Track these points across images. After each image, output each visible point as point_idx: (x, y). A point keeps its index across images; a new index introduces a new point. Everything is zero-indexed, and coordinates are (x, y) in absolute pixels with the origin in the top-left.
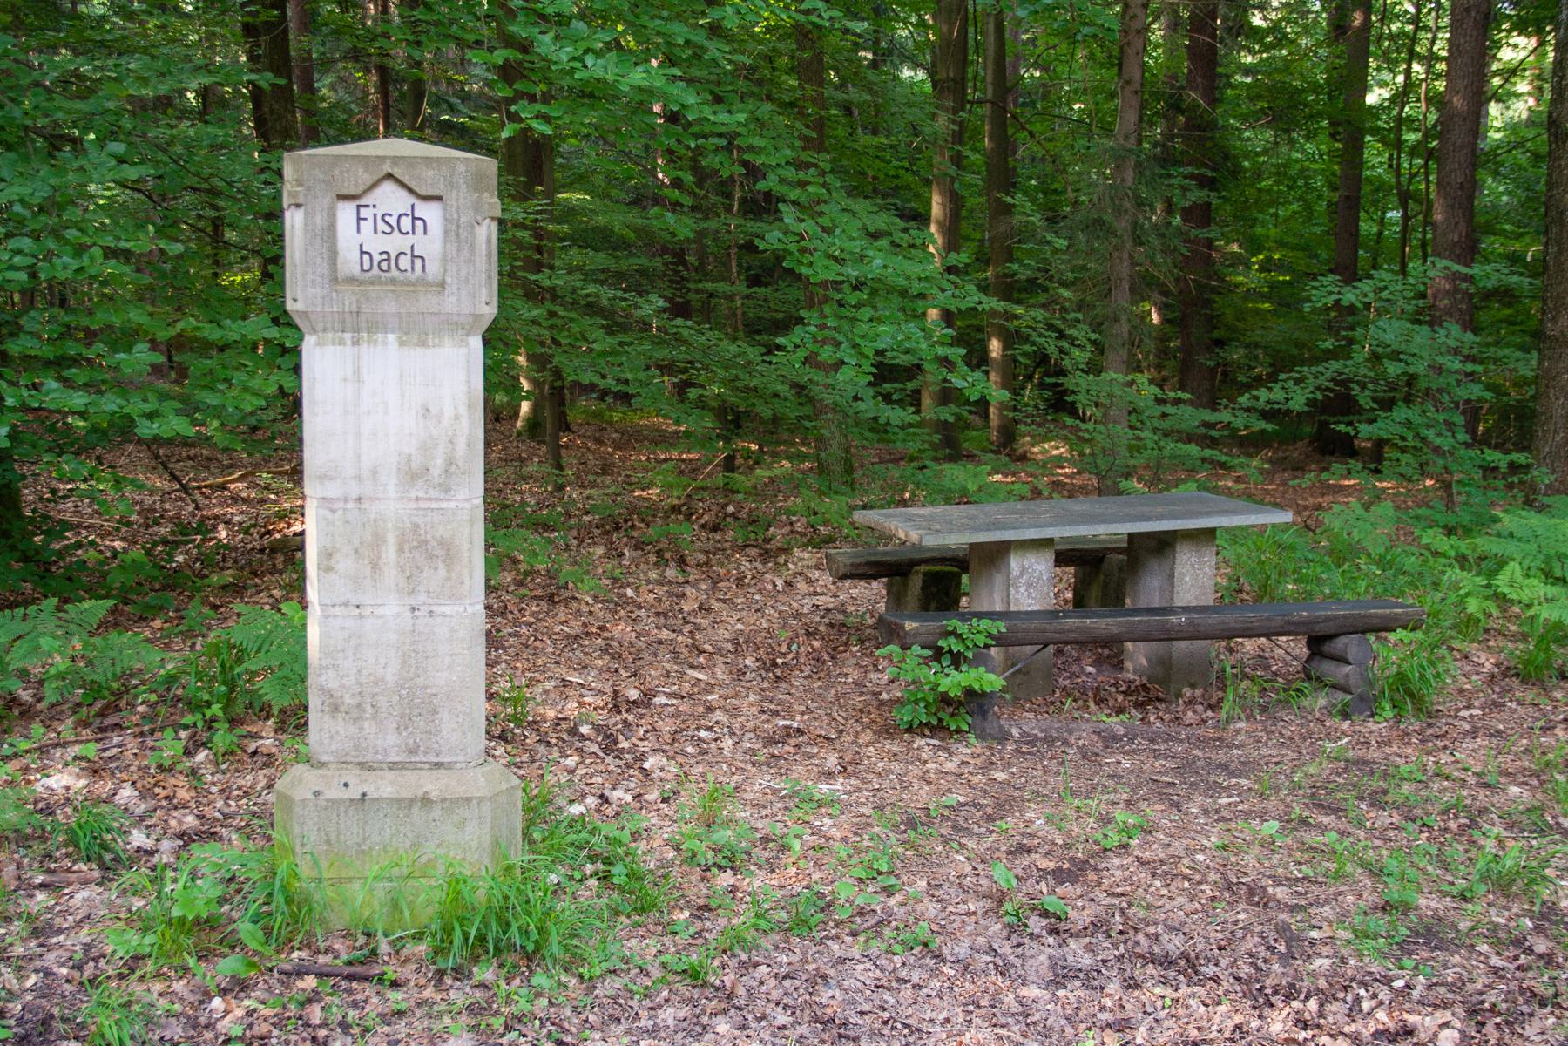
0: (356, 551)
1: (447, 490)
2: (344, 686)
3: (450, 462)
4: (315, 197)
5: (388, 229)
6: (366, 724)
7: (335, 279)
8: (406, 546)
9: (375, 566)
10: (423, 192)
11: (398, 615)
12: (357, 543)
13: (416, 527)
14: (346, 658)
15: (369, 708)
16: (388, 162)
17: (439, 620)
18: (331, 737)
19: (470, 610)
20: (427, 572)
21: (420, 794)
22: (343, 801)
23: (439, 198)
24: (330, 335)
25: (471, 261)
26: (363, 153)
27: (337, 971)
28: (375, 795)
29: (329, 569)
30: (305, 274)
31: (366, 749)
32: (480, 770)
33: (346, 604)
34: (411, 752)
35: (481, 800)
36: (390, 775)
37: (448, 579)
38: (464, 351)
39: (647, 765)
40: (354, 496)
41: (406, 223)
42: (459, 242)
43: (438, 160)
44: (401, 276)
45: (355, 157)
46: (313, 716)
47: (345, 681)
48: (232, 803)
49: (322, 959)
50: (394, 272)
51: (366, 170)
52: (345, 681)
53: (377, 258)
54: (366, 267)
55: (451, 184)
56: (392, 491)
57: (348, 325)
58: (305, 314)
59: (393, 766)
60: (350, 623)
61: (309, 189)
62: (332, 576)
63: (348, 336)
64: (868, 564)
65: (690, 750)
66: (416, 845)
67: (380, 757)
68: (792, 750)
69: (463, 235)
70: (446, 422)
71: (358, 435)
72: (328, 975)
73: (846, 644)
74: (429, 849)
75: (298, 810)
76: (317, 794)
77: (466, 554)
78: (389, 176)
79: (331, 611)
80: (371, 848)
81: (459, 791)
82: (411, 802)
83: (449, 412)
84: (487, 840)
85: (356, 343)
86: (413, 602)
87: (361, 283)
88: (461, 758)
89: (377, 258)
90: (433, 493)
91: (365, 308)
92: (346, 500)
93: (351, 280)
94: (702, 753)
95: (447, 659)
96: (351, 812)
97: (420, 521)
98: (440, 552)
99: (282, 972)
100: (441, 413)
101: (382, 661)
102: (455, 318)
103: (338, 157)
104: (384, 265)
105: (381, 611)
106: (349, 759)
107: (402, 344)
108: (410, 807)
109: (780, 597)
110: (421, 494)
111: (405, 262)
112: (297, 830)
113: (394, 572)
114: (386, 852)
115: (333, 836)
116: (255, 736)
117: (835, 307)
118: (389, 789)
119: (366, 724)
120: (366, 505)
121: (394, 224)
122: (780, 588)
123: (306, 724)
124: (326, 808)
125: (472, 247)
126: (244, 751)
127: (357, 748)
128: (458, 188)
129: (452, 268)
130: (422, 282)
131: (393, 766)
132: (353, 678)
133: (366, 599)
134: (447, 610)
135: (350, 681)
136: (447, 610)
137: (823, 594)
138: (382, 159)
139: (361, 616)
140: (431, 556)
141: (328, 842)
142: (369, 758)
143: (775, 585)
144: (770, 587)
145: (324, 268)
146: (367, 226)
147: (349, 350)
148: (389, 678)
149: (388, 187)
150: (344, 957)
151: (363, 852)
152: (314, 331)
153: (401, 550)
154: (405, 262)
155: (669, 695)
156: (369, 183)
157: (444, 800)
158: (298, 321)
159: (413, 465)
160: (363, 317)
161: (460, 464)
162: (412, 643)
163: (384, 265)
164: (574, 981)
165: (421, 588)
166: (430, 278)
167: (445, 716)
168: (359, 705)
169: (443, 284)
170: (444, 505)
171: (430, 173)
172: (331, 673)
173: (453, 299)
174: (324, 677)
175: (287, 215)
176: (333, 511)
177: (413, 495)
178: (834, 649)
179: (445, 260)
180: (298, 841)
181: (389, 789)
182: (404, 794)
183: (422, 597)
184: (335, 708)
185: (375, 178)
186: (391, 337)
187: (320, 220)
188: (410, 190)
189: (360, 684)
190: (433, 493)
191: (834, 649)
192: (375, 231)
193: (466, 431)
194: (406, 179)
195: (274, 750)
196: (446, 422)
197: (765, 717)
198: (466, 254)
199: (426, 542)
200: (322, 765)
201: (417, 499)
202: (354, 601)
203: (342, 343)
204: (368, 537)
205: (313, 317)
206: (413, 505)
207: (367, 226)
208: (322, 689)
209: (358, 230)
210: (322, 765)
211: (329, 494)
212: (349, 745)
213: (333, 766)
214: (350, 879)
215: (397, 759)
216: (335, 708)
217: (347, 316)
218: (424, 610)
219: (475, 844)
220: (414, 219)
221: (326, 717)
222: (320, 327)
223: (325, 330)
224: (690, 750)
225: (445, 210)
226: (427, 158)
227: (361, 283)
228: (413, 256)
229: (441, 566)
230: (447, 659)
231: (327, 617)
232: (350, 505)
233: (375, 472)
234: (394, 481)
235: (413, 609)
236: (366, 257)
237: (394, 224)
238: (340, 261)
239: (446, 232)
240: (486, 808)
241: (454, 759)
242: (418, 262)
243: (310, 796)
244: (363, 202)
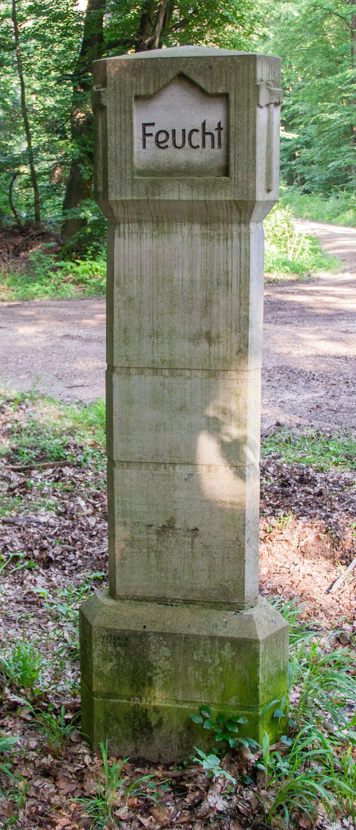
209: (144, 147)
228: (204, 133)
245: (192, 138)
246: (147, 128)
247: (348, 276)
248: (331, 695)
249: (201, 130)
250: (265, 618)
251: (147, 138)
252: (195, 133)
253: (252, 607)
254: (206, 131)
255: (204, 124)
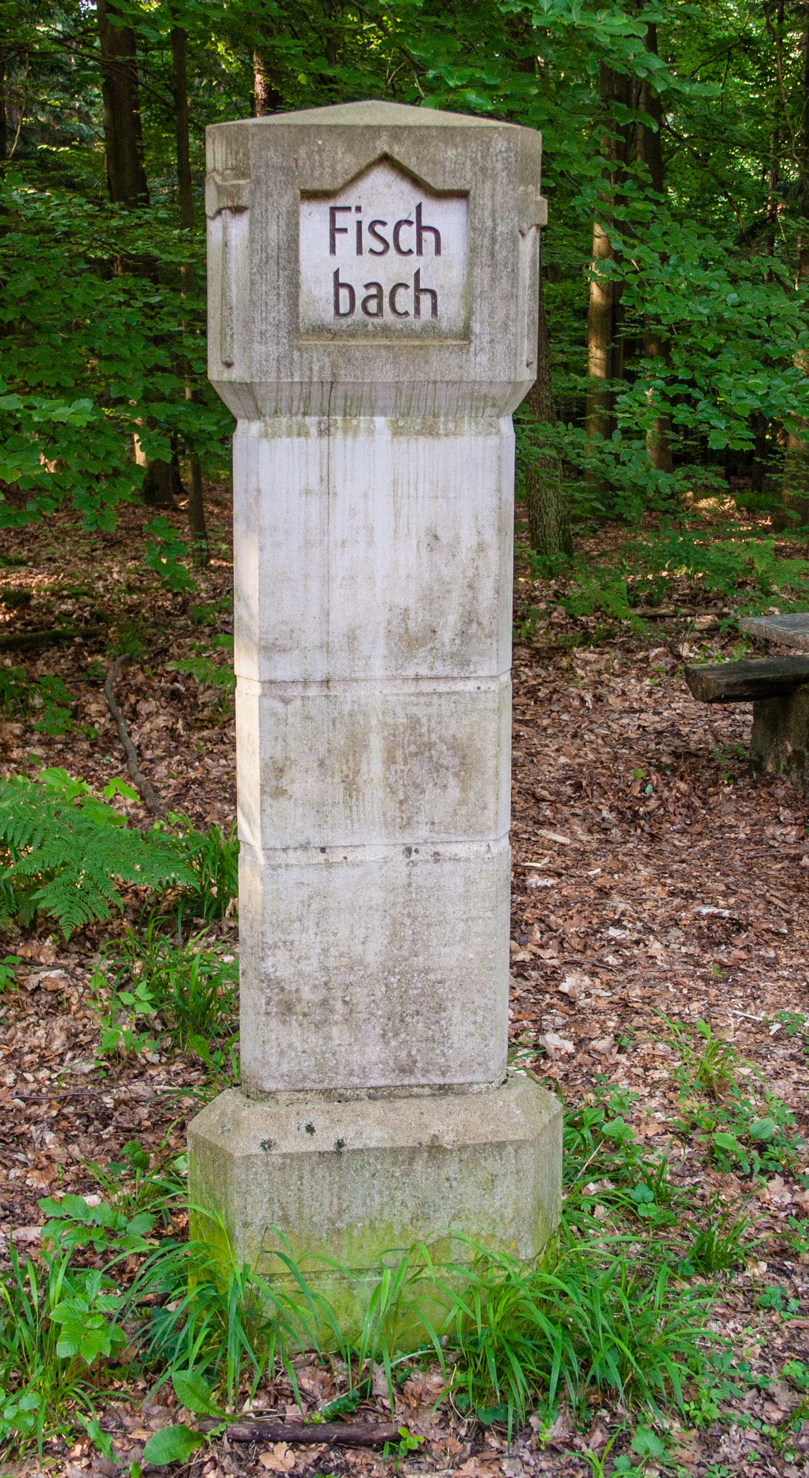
0: (322, 764)
1: (465, 663)
2: (300, 974)
3: (469, 618)
4: (268, 195)
5: (379, 247)
6: (335, 1031)
7: (295, 331)
8: (399, 753)
9: (351, 786)
10: (439, 183)
11: (386, 861)
12: (322, 750)
13: (414, 723)
14: (304, 930)
15: (339, 1005)
16: (385, 136)
17: (448, 866)
18: (282, 1053)
19: (495, 850)
20: (431, 793)
21: (426, 1139)
22: (309, 1155)
23: (462, 195)
24: (284, 420)
25: (511, 297)
26: (342, 121)
27: (320, 1433)
28: (357, 1145)
29: (279, 793)
30: (248, 324)
31: (335, 1069)
32: (506, 1093)
33: (305, 847)
34: (404, 1070)
35: (519, 1145)
36: (376, 1109)
37: (463, 802)
38: (493, 441)
39: (564, 987)
40: (319, 676)
41: (408, 236)
42: (494, 265)
43: (464, 130)
44: (398, 323)
45: (332, 128)
46: (247, 1020)
47: (303, 965)
48: (29, 1076)
49: (293, 1412)
50: (388, 316)
51: (350, 149)
52: (303, 965)
53: (361, 293)
54: (344, 308)
55: (483, 169)
56: (378, 668)
57: (315, 403)
58: (247, 389)
59: (375, 1094)
60: (311, 876)
61: (258, 182)
62: (283, 803)
63: (312, 421)
64: (747, 683)
65: (611, 960)
66: (421, 1216)
67: (356, 1081)
68: (743, 955)
69: (501, 255)
70: (464, 555)
71: (327, 580)
72: (308, 1441)
73: (715, 784)
74: (440, 1225)
75: (238, 1172)
76: (267, 1145)
77: (491, 763)
78: (386, 159)
79: (281, 858)
80: (350, 1226)
81: (486, 1132)
82: (413, 1153)
83: (468, 540)
84: (528, 1203)
85: (325, 432)
86: (409, 841)
87: (335, 335)
88: (479, 1077)
89: (361, 293)
90: (441, 669)
91: (346, 376)
92: (306, 683)
93: (319, 330)
94: (628, 963)
95: (461, 926)
96: (319, 1172)
97: (420, 712)
98: (449, 760)
99: (236, 1440)
100: (457, 539)
101: (361, 933)
102: (484, 390)
103: (304, 129)
104: (372, 306)
105: (355, 856)
106: (308, 1085)
107: (397, 432)
108: (411, 1160)
109: (593, 717)
110: (424, 671)
111: (405, 300)
112: (237, 1202)
113: (380, 794)
114: (373, 1229)
115: (292, 1212)
116: (30, 962)
117: (685, 355)
118: (378, 1133)
119: (335, 1031)
120: (337, 690)
121: (390, 240)
122: (589, 704)
123: (236, 1029)
124: (282, 1168)
125: (514, 272)
126: (22, 987)
127: (320, 1067)
128: (494, 177)
129: (482, 309)
130: (432, 331)
131: (375, 1094)
132: (314, 961)
133: (337, 837)
134: (460, 850)
135: (310, 966)
136: (460, 850)
137: (641, 711)
138: (375, 131)
139: (329, 865)
140: (438, 768)
141: (285, 1219)
142: (339, 1081)
143: (583, 701)
144: (576, 703)
145: (280, 313)
146: (347, 242)
147: (314, 443)
148: (370, 958)
149: (381, 178)
150: (325, 1406)
151: (339, 1232)
152: (259, 414)
153: (390, 760)
154: (405, 300)
155: (543, 873)
156: (353, 171)
157: (463, 1148)
158: (228, 399)
159: (411, 625)
160: (340, 390)
161: (485, 621)
162: (406, 905)
163: (372, 306)
164: (677, 1425)
165: (422, 818)
166: (444, 325)
167: (456, 1014)
168: (324, 1002)
169: (466, 334)
170: (459, 686)
171: (451, 153)
172: (281, 955)
173: (483, 358)
174: (270, 961)
175: (214, 228)
176: (286, 701)
177: (411, 673)
178: (704, 791)
179: (469, 295)
180: (238, 1221)
181: (378, 1133)
182: (401, 1142)
183: (423, 832)
184: (288, 1008)
185: (364, 164)
186: (380, 421)
187: (274, 233)
188: (416, 182)
189: (326, 969)
190: (441, 669)
191: (704, 791)
192: (360, 251)
193: (494, 569)
194: (412, 164)
195: (62, 985)
196: (464, 555)
197: (677, 901)
198: (504, 284)
199: (430, 746)
200: (265, 1096)
201: (417, 678)
202: (317, 841)
203: (302, 432)
204: (341, 741)
205: (260, 392)
206: (411, 688)
207: (347, 242)
208: (267, 980)
209: (333, 250)
210: (265, 1096)
211: (280, 675)
212: (308, 1064)
213: (283, 1097)
214: (318, 1274)
215: (382, 1082)
216: (288, 1008)
217: (315, 390)
218: (426, 851)
219: (509, 1213)
220: (421, 229)
221: (274, 1022)
222: (269, 407)
223: (276, 412)
224: (611, 960)
225: (470, 212)
226: (445, 128)
227: (335, 335)
228: (418, 290)
229: (452, 781)
230: (461, 926)
231: (274, 868)
232: (313, 691)
233: (352, 638)
234: (381, 650)
235: (409, 851)
236: (343, 293)
237: (390, 240)
238: (303, 299)
239: (473, 250)
240: (528, 1157)
241: (469, 1079)
242: (426, 300)
243: (256, 1150)
244: (340, 202)
245: (401, 233)
246: (339, 216)
247: (802, 543)
248: (739, 560)
249: (411, 283)
250: (223, 1114)
251: (338, 236)
252: (401, 291)
253: (248, 1096)
254: (422, 286)
255: (417, 274)
